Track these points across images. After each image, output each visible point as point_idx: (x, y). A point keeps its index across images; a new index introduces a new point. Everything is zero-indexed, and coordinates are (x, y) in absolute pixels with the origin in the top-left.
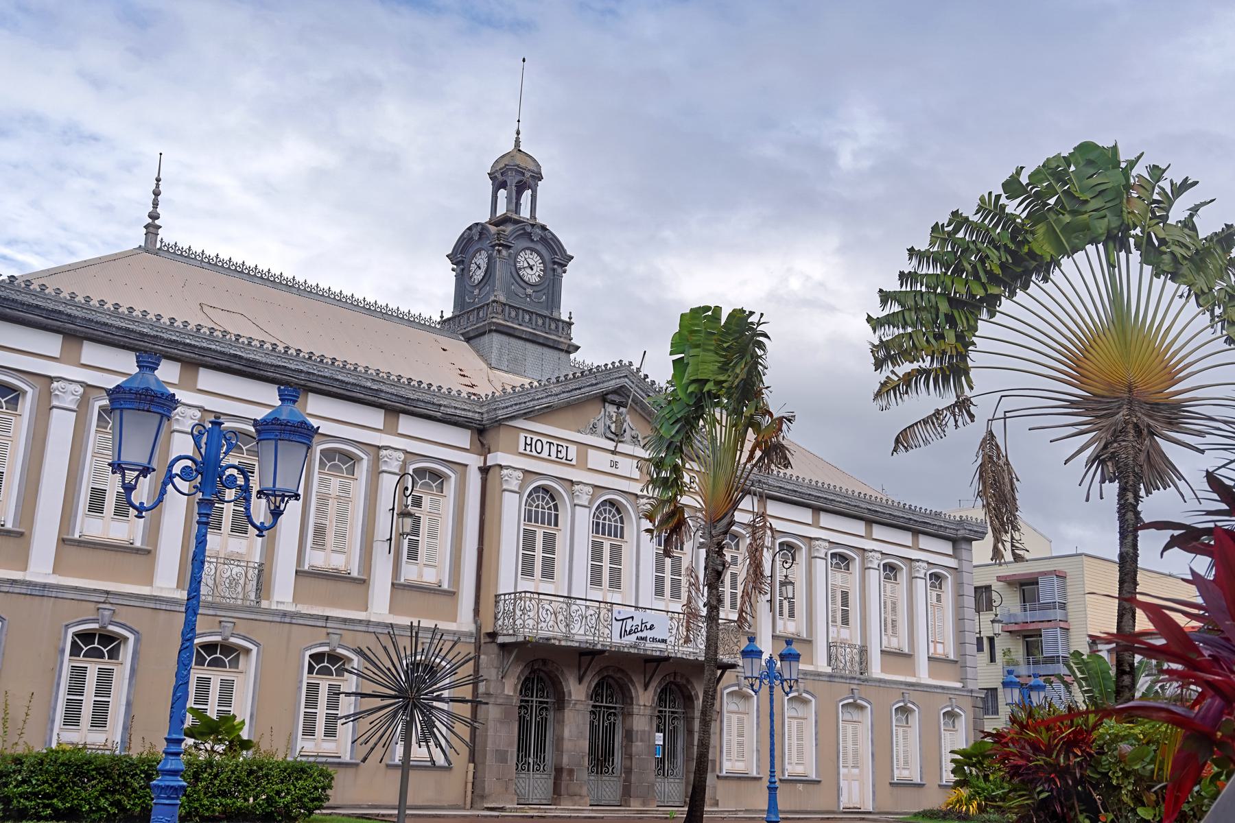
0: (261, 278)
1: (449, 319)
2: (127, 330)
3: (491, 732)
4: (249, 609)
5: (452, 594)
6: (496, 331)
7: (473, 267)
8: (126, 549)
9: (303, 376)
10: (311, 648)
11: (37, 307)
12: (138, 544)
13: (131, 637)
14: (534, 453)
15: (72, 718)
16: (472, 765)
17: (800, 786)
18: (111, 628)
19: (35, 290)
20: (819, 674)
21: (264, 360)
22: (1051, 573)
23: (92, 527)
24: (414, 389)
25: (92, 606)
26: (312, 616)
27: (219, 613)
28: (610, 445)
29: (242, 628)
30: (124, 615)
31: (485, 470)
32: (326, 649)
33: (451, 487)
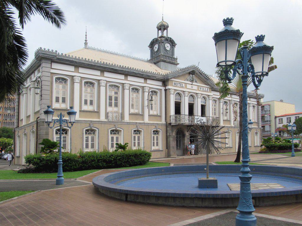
0: (110, 53)
1: (150, 60)
2: (88, 64)
3: (171, 143)
4: (121, 122)
5: (160, 116)
6: (162, 61)
7: (154, 48)
8: (94, 112)
9: (127, 72)
10: (134, 129)
11: (68, 60)
12: (96, 110)
13: (97, 130)
14: (176, 86)
15: (87, 147)
16: (167, 150)
17: (229, 148)
18: (93, 128)
19: (67, 56)
20: (232, 127)
21: (118, 69)
22: (267, 105)
23: (85, 108)
24: (150, 73)
25: (88, 124)
26: (133, 123)
27: (114, 123)
28: (191, 83)
29: (119, 126)
30: (95, 125)
31: (166, 90)
32: (136, 129)
33: (159, 94)
